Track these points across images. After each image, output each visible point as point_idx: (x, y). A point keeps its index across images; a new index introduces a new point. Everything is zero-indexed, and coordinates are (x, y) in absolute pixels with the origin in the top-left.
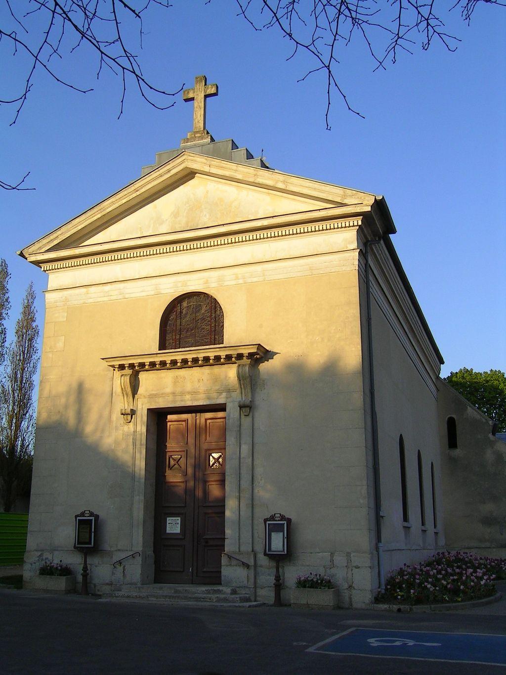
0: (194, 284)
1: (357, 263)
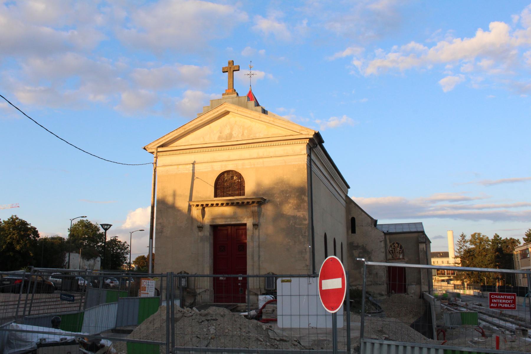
0: (230, 167)
1: (306, 160)
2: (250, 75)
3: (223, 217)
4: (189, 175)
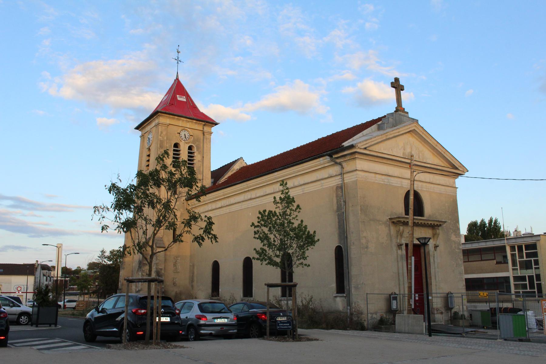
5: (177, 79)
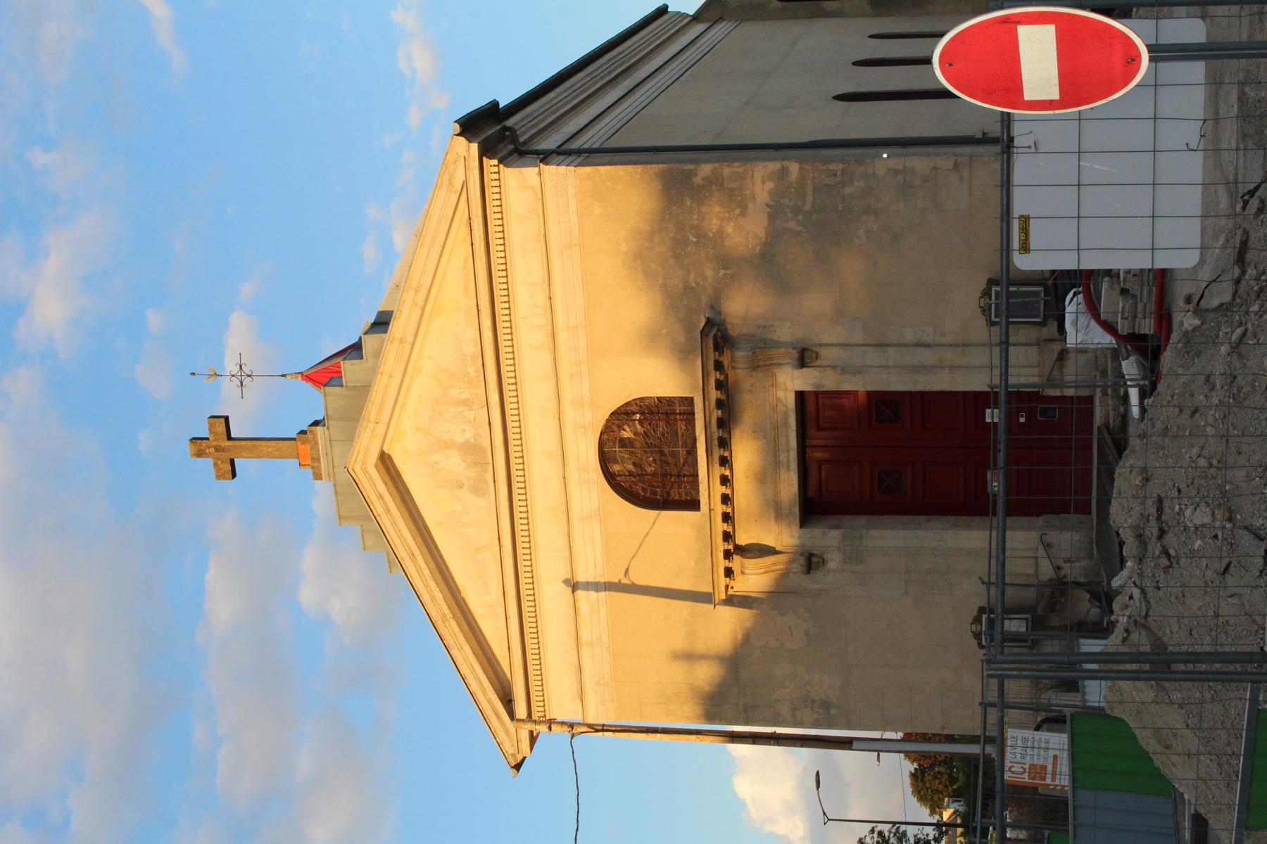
0: (586, 451)
1: (562, 169)
2: (243, 376)
3: (766, 477)
4: (618, 599)
5: (308, 377)
